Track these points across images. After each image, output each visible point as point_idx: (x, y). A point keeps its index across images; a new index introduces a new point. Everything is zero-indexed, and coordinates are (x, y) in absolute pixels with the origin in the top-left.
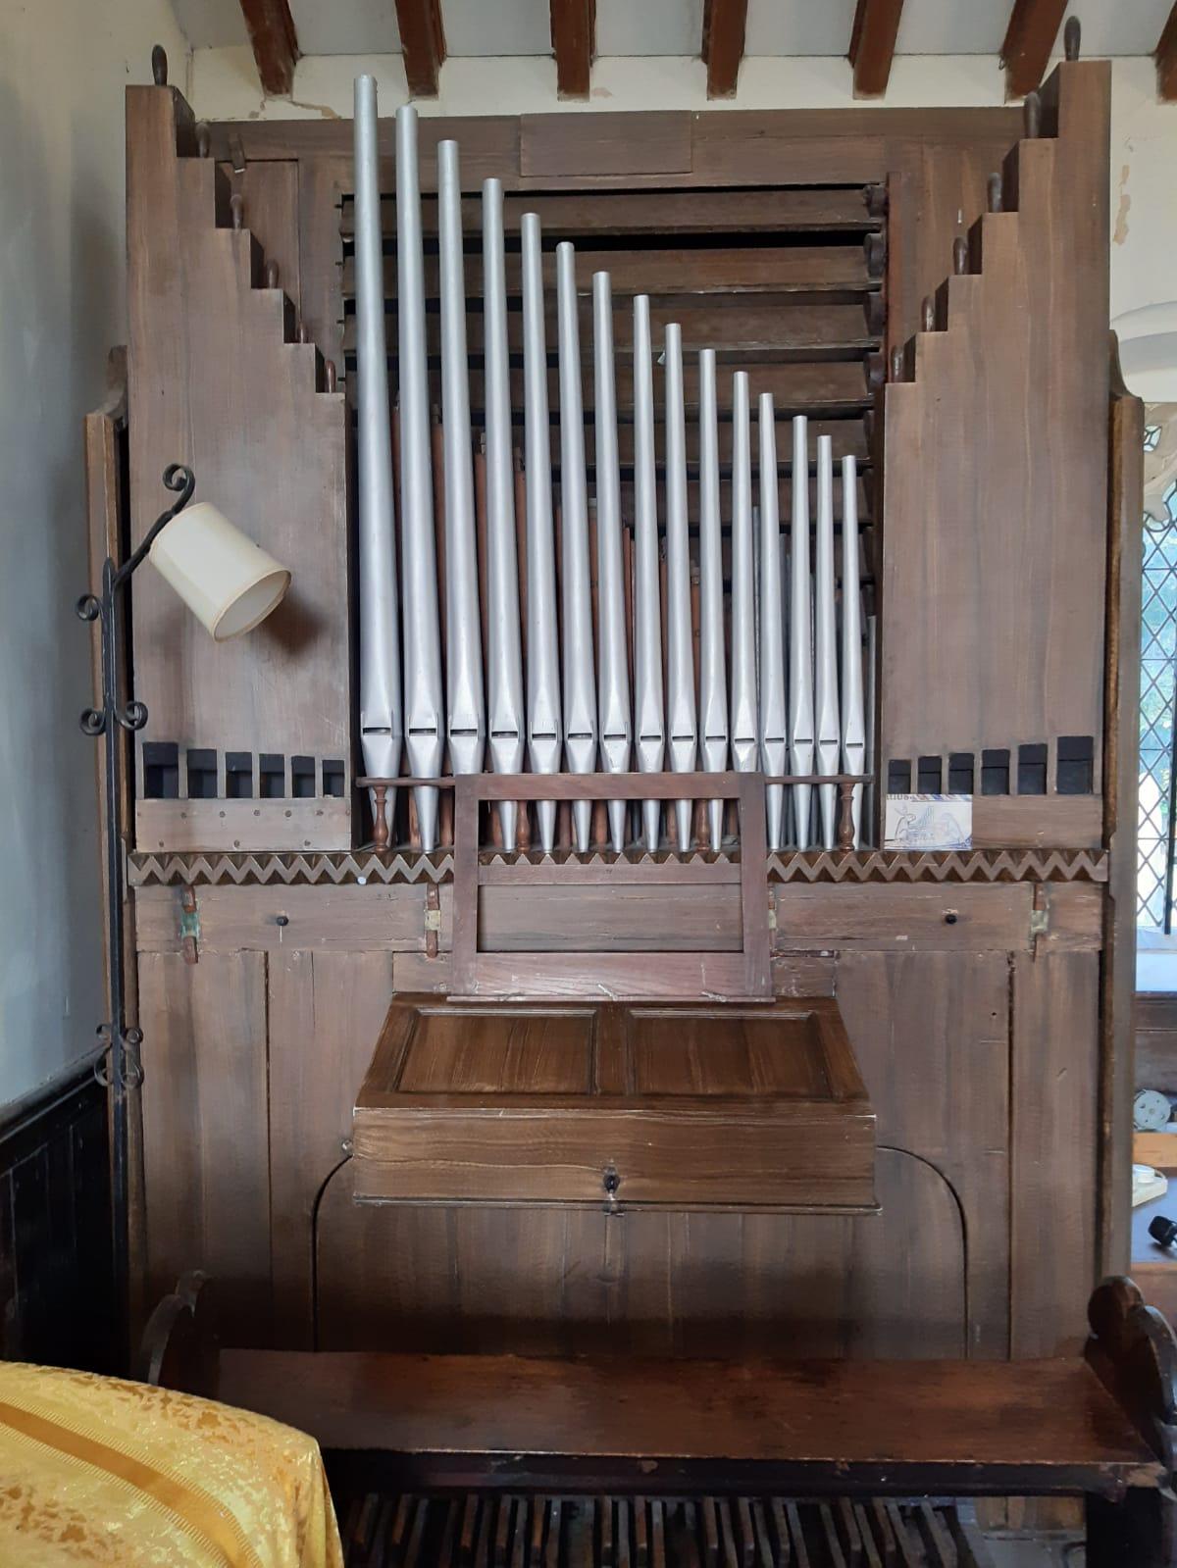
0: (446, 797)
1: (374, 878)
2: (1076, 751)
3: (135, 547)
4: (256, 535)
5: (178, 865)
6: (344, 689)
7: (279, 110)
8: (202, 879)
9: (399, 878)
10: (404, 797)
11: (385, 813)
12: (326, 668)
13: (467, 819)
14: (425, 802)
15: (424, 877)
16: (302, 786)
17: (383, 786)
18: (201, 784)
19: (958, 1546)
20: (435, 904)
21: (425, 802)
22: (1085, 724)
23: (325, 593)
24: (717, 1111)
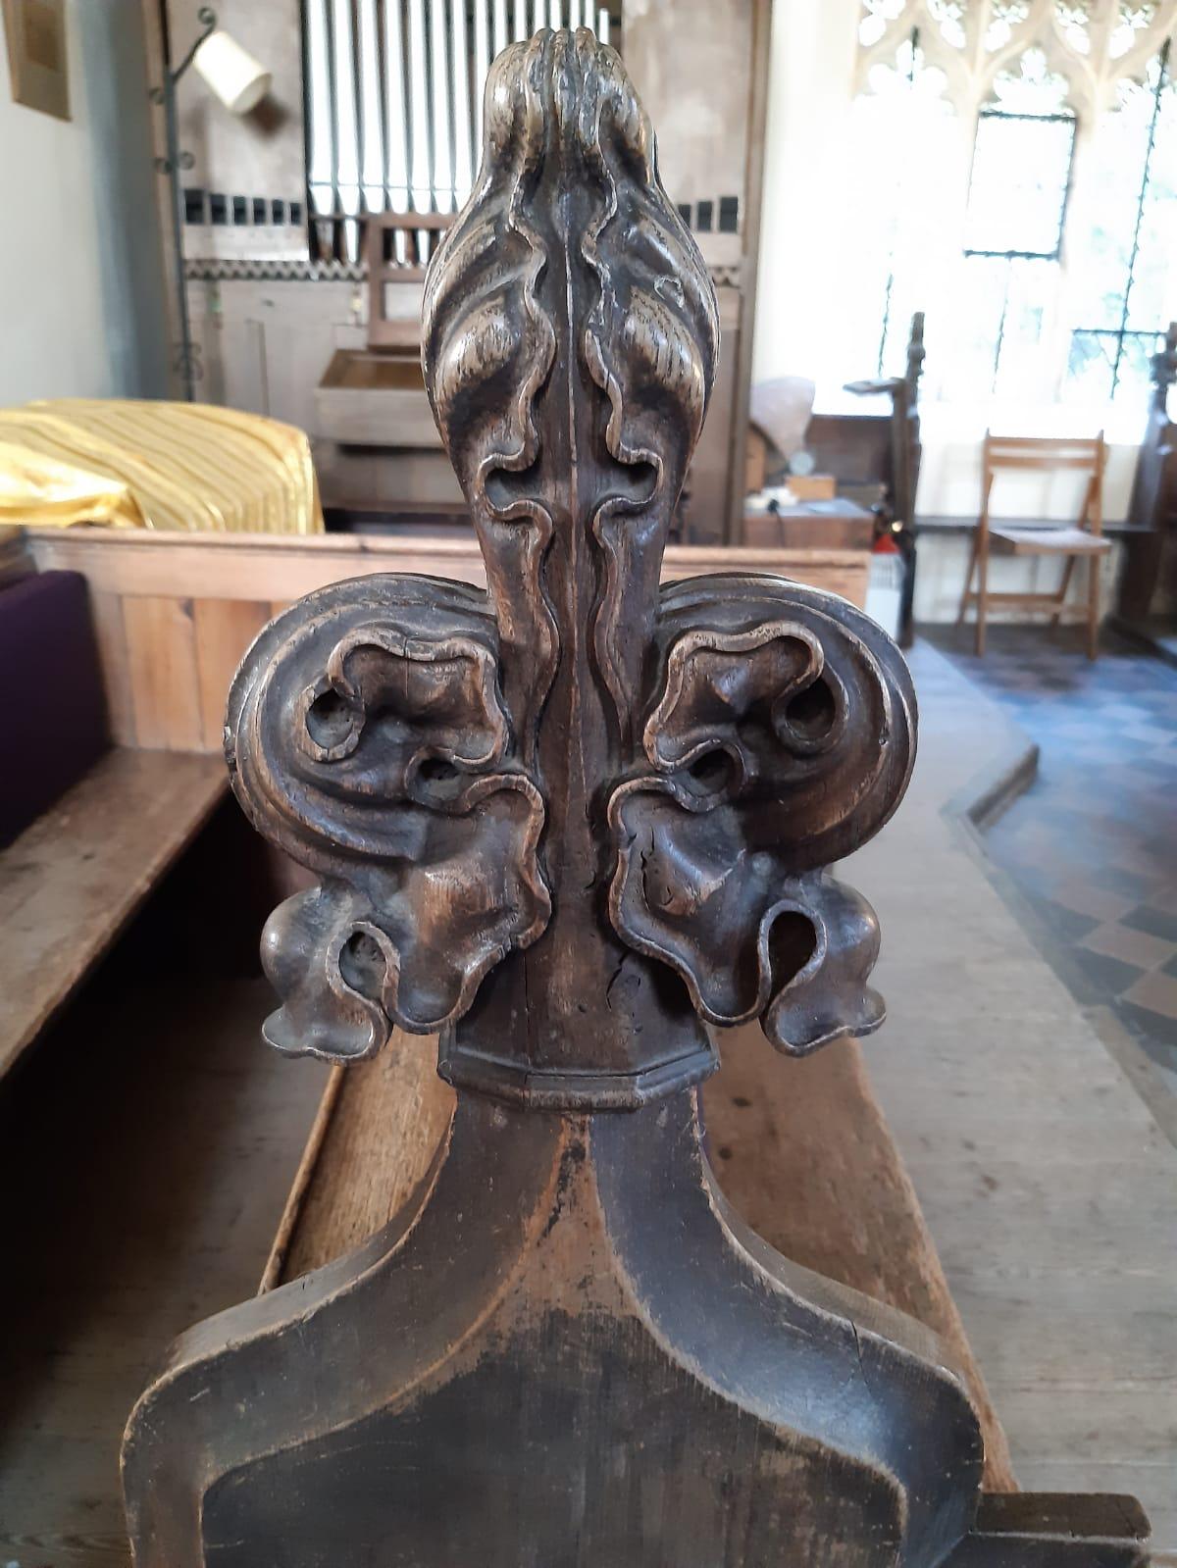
0: (363, 226)
1: (322, 277)
2: (729, 206)
3: (176, 63)
4: (252, 52)
5: (207, 267)
6: (300, 155)
7: (529, 131)
8: (222, 275)
9: (336, 277)
10: (338, 225)
11: (327, 235)
12: (288, 143)
13: (375, 239)
14: (351, 230)
15: (351, 277)
16: (278, 216)
17: (325, 219)
18: (218, 215)
19: (544, 383)
20: (357, 294)
21: (351, 230)
22: (734, 187)
23: (286, 94)
24: (614, 641)
